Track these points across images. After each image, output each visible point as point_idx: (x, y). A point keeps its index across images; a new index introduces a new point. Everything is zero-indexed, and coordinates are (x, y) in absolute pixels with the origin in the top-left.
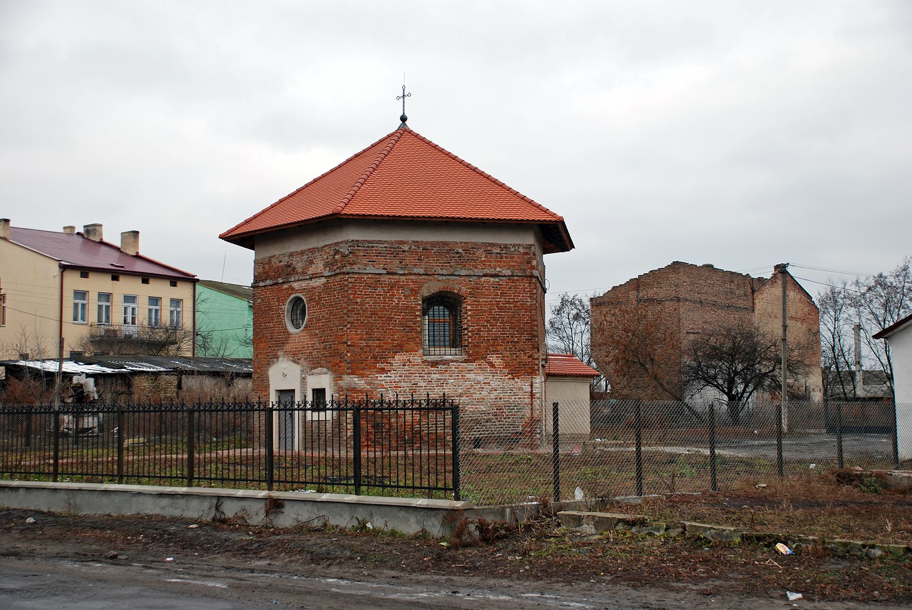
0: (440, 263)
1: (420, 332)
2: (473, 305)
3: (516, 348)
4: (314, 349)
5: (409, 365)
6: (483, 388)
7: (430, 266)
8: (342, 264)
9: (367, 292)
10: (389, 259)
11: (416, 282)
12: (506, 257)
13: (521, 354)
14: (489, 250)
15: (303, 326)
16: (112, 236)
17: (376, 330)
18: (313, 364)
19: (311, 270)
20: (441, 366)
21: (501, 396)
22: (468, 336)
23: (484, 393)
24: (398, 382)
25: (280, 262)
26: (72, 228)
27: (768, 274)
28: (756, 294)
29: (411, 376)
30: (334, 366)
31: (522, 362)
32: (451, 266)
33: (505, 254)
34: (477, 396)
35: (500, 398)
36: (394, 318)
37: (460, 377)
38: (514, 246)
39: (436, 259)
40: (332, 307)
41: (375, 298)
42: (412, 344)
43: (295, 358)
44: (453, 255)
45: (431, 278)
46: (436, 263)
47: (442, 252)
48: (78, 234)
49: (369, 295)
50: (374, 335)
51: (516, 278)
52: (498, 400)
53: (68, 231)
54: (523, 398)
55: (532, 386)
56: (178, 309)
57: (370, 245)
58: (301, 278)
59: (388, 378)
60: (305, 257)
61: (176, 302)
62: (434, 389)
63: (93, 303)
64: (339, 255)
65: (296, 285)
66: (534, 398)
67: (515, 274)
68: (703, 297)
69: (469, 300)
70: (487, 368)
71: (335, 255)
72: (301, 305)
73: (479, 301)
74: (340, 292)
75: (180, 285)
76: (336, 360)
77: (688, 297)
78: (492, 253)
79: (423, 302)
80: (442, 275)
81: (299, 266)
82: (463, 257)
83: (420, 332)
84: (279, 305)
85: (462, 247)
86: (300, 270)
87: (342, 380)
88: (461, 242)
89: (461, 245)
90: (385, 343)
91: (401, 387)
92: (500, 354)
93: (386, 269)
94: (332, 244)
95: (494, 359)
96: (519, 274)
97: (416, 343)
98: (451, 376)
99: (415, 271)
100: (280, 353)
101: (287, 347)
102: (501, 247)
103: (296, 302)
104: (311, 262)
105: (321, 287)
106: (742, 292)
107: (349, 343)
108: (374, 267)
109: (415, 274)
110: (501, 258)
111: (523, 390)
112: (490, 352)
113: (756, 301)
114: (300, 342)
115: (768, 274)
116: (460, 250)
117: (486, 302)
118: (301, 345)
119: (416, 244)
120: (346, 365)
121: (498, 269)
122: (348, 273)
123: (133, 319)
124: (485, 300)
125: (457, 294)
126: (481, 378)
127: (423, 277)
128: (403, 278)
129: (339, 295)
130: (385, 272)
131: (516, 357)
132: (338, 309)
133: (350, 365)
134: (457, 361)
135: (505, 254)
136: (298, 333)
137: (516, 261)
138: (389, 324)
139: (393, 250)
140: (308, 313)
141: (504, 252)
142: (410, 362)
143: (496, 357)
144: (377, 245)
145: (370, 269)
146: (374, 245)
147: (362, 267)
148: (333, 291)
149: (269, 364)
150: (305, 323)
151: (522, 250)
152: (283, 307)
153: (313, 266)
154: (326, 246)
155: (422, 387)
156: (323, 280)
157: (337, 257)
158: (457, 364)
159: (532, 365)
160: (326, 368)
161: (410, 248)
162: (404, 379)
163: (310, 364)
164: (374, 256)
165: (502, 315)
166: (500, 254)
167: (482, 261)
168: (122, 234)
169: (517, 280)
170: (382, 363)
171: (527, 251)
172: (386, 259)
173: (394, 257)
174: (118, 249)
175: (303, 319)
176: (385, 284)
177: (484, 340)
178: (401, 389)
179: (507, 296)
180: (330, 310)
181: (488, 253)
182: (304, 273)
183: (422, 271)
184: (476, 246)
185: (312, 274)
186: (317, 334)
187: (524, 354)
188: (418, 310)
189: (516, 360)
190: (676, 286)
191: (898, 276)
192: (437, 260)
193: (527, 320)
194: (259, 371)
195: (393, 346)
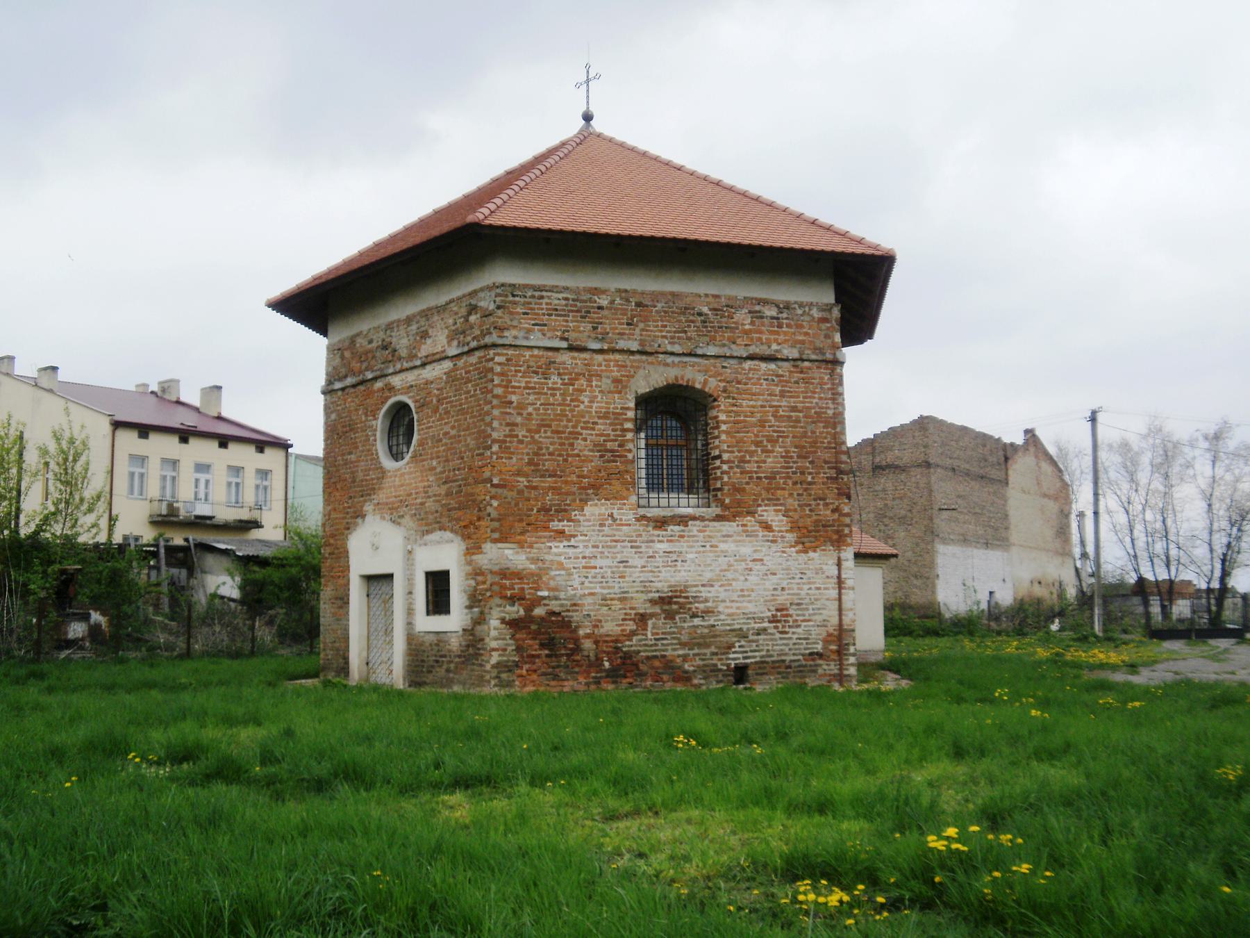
0: (667, 332)
1: (633, 462)
2: (730, 412)
3: (810, 495)
4: (429, 497)
5: (610, 525)
6: (751, 570)
7: (649, 336)
8: (482, 331)
9: (530, 382)
10: (572, 321)
11: (623, 366)
12: (788, 326)
13: (819, 504)
14: (756, 312)
15: (410, 454)
16: (190, 395)
17: (547, 457)
18: (427, 524)
19: (426, 349)
20: (672, 527)
21: (784, 584)
22: (725, 472)
23: (753, 579)
24: (590, 558)
25: (371, 342)
26: (146, 385)
27: (1019, 440)
28: (1010, 462)
29: (615, 547)
30: (465, 527)
31: (820, 521)
32: (689, 339)
33: (787, 318)
34: (737, 585)
35: (783, 589)
36: (581, 434)
37: (708, 548)
38: (801, 305)
39: (660, 323)
40: (463, 414)
41: (546, 394)
42: (616, 485)
43: (394, 513)
44: (691, 318)
45: (651, 359)
46: (661, 331)
47: (673, 312)
48: (152, 392)
49: (535, 388)
50: (544, 465)
51: (807, 364)
52: (779, 592)
53: (141, 389)
54: (826, 589)
55: (839, 564)
56: (265, 483)
57: (537, 294)
58: (406, 365)
59: (571, 551)
60: (414, 327)
61: (264, 474)
62: (660, 572)
63: (154, 471)
64: (476, 313)
65: (396, 381)
66: (845, 588)
67: (805, 357)
68: (956, 463)
69: (723, 403)
70: (757, 531)
71: (469, 314)
72: (407, 420)
73: (741, 406)
74: (477, 385)
75: (269, 452)
76: (471, 515)
77: (940, 463)
78: (762, 317)
79: (637, 405)
80: (672, 354)
81: (402, 342)
82: (711, 322)
83: (633, 462)
84: (367, 420)
85: (708, 304)
86: (404, 353)
87: (481, 553)
88: (707, 295)
89: (708, 300)
90: (566, 482)
91: (596, 568)
92: (781, 505)
93: (566, 339)
94: (464, 296)
95: (770, 514)
96: (814, 357)
97: (623, 484)
98: (692, 547)
99: (622, 344)
100: (368, 508)
101: (381, 496)
102: (777, 306)
103: (398, 412)
104: (424, 335)
105: (441, 378)
106: (995, 460)
107: (495, 481)
108: (544, 335)
109: (621, 351)
110: (780, 326)
111: (823, 573)
112: (763, 501)
113: (1010, 472)
114: (402, 485)
115: (1019, 440)
116: (705, 310)
117: (753, 407)
118: (405, 490)
119: (623, 295)
120: (489, 523)
121: (774, 347)
122: (494, 346)
123: (206, 495)
124: (751, 403)
125: (701, 392)
126: (746, 550)
127: (637, 357)
128: (600, 358)
129: (475, 390)
130: (564, 344)
131: (811, 510)
132: (475, 417)
133: (496, 524)
134: (702, 519)
135: (787, 318)
136: (399, 470)
137: (806, 334)
138: (572, 445)
139: (578, 304)
140: (419, 430)
141: (785, 315)
142: (614, 520)
143: (775, 510)
144: (549, 294)
145: (536, 339)
146: (544, 294)
147: (521, 334)
148: (466, 383)
149: (348, 529)
150: (412, 449)
151: (816, 313)
152: (374, 422)
153: (429, 341)
154: (451, 301)
155: (636, 567)
156: (447, 365)
157: (473, 318)
158: (703, 524)
159: (839, 526)
160: (452, 531)
161: (612, 302)
162: (602, 553)
163: (421, 525)
164: (544, 314)
165: (784, 432)
166: (777, 318)
167: (747, 332)
168: (202, 389)
169: (810, 368)
170: (559, 521)
171: (825, 315)
172: (567, 321)
173: (582, 317)
174: (197, 410)
175: (409, 443)
176: (564, 368)
177: (751, 478)
178: (598, 571)
179: (791, 397)
180: (460, 420)
181: (757, 317)
182: (412, 357)
183: (634, 346)
184: (732, 305)
185: (426, 357)
186: (434, 468)
187: (826, 505)
188: (627, 420)
189: (810, 516)
190: (925, 447)
191: (1175, 447)
192: (662, 326)
193: (829, 443)
194: (332, 541)
195: (580, 488)
